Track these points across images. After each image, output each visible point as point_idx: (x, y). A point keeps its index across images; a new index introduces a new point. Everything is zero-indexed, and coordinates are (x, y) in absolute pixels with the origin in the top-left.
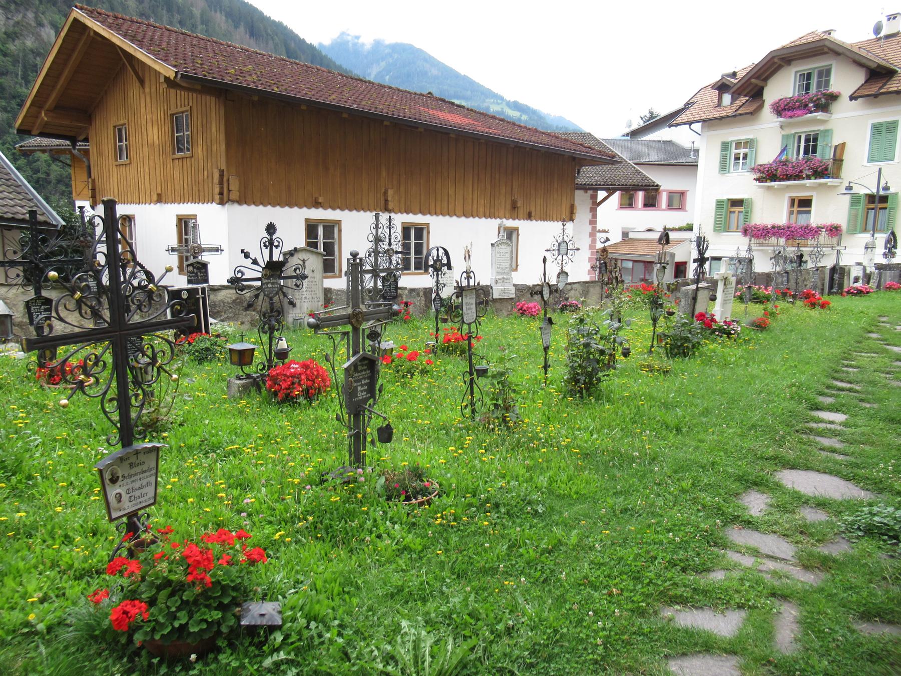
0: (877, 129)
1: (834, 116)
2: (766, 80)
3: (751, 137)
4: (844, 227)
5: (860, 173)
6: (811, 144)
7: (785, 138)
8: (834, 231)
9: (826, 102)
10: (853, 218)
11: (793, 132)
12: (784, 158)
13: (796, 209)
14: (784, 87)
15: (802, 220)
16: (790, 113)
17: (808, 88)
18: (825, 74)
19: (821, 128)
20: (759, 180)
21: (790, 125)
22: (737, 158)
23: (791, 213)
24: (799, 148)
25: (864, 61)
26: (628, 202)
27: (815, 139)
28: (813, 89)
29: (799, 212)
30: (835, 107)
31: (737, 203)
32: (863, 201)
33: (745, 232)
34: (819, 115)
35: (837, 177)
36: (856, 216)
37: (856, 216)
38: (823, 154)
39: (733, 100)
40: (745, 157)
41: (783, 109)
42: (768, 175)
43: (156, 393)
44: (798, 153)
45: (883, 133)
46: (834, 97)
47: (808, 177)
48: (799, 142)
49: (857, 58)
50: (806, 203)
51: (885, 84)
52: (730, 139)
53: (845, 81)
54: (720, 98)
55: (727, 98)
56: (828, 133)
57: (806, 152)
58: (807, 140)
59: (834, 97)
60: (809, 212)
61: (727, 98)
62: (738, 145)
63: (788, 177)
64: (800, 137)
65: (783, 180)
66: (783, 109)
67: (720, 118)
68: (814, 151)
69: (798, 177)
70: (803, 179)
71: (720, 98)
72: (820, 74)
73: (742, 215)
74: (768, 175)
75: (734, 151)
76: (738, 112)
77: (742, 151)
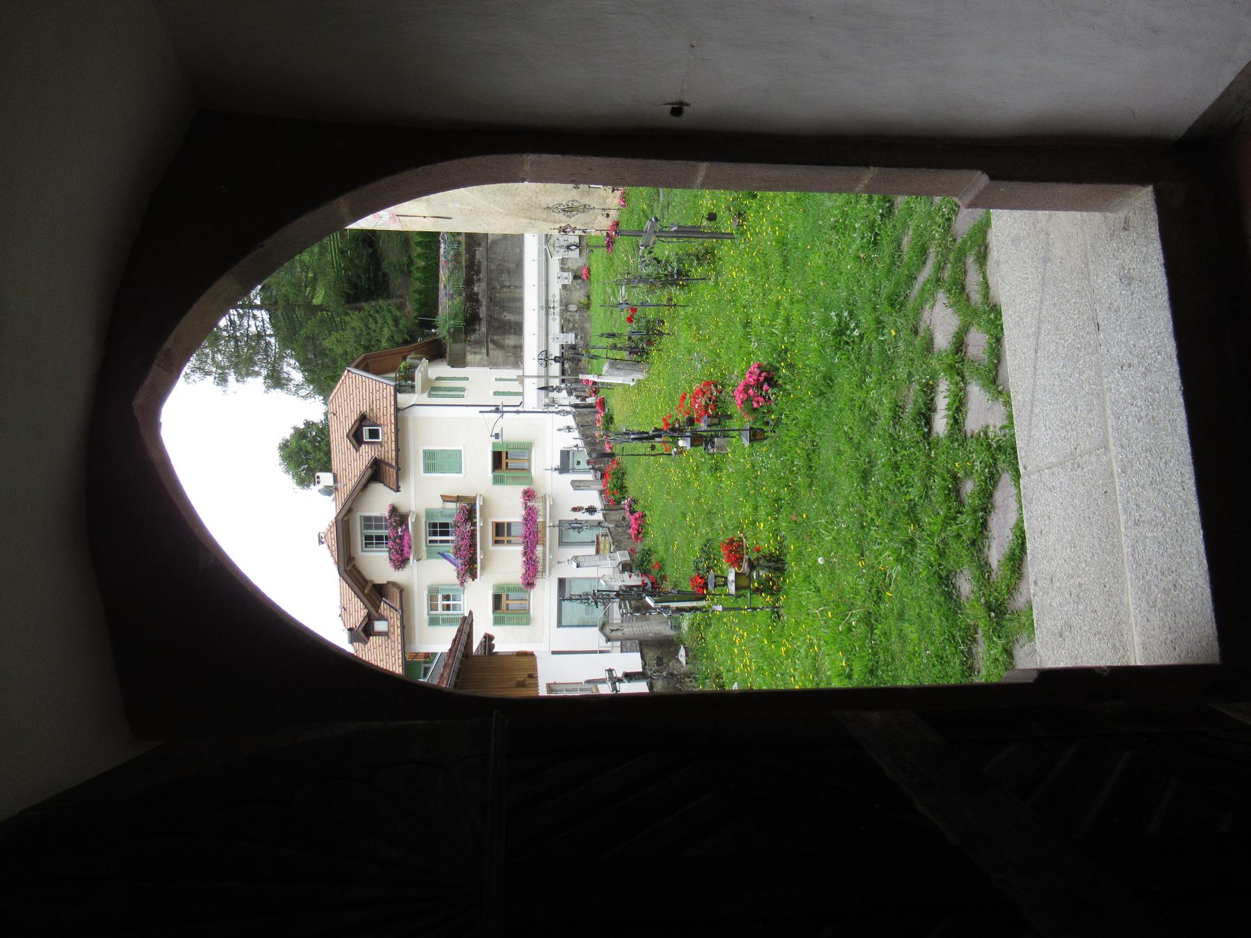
0: (429, 468)
1: (413, 509)
2: (366, 582)
3: (426, 592)
4: (526, 487)
5: (475, 475)
6: (438, 529)
7: (430, 555)
8: (529, 495)
9: (398, 517)
10: (516, 480)
11: (424, 548)
12: (452, 556)
13: (505, 538)
14: (378, 565)
15: (518, 531)
16: (406, 549)
17: (379, 538)
18: (368, 522)
19: (423, 520)
20: (474, 577)
21: (417, 552)
22: (448, 607)
23: (509, 542)
24: (441, 541)
25: (364, 481)
26: (480, 253)
27: (434, 525)
28: (384, 532)
29: (509, 534)
30: (403, 509)
31: (497, 599)
32: (499, 473)
33: (530, 584)
34: (411, 520)
35: (475, 499)
36: (514, 478)
37: (514, 478)
38: (450, 516)
39: (382, 618)
40: (447, 598)
41: (400, 561)
42: (469, 569)
43: (555, 326)
44: (447, 541)
45: (433, 462)
46: (394, 510)
47: (474, 524)
48: (436, 541)
49: (359, 488)
50: (500, 529)
51: (388, 464)
52: (426, 617)
53: (380, 501)
54: (379, 634)
55: (380, 626)
56: (429, 513)
57: (446, 533)
58: (435, 534)
59: (394, 510)
60: (509, 524)
61: (380, 626)
62: (433, 607)
63: (473, 546)
64: (431, 542)
65: (475, 550)
66: (400, 561)
67: (403, 627)
68: (446, 525)
69: (473, 535)
70: (474, 531)
71: (379, 634)
72: (368, 527)
73: (512, 596)
74: (469, 569)
75: (440, 611)
76: (398, 606)
77: (441, 602)
